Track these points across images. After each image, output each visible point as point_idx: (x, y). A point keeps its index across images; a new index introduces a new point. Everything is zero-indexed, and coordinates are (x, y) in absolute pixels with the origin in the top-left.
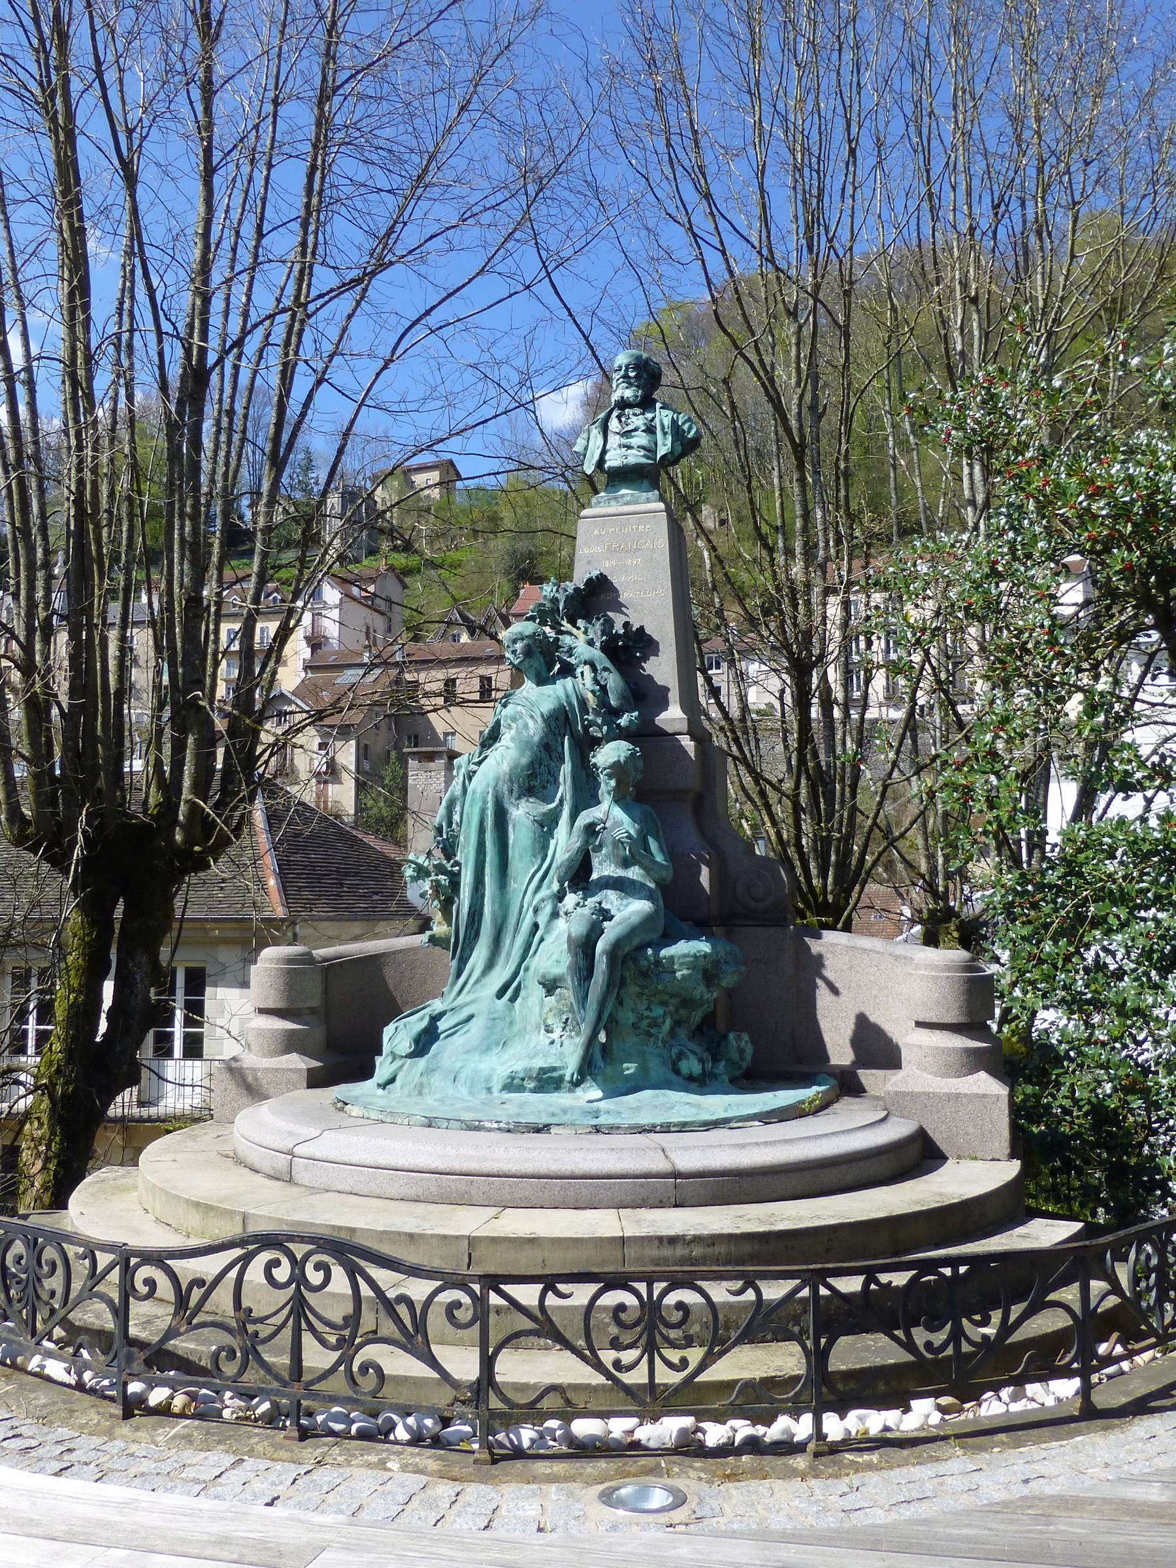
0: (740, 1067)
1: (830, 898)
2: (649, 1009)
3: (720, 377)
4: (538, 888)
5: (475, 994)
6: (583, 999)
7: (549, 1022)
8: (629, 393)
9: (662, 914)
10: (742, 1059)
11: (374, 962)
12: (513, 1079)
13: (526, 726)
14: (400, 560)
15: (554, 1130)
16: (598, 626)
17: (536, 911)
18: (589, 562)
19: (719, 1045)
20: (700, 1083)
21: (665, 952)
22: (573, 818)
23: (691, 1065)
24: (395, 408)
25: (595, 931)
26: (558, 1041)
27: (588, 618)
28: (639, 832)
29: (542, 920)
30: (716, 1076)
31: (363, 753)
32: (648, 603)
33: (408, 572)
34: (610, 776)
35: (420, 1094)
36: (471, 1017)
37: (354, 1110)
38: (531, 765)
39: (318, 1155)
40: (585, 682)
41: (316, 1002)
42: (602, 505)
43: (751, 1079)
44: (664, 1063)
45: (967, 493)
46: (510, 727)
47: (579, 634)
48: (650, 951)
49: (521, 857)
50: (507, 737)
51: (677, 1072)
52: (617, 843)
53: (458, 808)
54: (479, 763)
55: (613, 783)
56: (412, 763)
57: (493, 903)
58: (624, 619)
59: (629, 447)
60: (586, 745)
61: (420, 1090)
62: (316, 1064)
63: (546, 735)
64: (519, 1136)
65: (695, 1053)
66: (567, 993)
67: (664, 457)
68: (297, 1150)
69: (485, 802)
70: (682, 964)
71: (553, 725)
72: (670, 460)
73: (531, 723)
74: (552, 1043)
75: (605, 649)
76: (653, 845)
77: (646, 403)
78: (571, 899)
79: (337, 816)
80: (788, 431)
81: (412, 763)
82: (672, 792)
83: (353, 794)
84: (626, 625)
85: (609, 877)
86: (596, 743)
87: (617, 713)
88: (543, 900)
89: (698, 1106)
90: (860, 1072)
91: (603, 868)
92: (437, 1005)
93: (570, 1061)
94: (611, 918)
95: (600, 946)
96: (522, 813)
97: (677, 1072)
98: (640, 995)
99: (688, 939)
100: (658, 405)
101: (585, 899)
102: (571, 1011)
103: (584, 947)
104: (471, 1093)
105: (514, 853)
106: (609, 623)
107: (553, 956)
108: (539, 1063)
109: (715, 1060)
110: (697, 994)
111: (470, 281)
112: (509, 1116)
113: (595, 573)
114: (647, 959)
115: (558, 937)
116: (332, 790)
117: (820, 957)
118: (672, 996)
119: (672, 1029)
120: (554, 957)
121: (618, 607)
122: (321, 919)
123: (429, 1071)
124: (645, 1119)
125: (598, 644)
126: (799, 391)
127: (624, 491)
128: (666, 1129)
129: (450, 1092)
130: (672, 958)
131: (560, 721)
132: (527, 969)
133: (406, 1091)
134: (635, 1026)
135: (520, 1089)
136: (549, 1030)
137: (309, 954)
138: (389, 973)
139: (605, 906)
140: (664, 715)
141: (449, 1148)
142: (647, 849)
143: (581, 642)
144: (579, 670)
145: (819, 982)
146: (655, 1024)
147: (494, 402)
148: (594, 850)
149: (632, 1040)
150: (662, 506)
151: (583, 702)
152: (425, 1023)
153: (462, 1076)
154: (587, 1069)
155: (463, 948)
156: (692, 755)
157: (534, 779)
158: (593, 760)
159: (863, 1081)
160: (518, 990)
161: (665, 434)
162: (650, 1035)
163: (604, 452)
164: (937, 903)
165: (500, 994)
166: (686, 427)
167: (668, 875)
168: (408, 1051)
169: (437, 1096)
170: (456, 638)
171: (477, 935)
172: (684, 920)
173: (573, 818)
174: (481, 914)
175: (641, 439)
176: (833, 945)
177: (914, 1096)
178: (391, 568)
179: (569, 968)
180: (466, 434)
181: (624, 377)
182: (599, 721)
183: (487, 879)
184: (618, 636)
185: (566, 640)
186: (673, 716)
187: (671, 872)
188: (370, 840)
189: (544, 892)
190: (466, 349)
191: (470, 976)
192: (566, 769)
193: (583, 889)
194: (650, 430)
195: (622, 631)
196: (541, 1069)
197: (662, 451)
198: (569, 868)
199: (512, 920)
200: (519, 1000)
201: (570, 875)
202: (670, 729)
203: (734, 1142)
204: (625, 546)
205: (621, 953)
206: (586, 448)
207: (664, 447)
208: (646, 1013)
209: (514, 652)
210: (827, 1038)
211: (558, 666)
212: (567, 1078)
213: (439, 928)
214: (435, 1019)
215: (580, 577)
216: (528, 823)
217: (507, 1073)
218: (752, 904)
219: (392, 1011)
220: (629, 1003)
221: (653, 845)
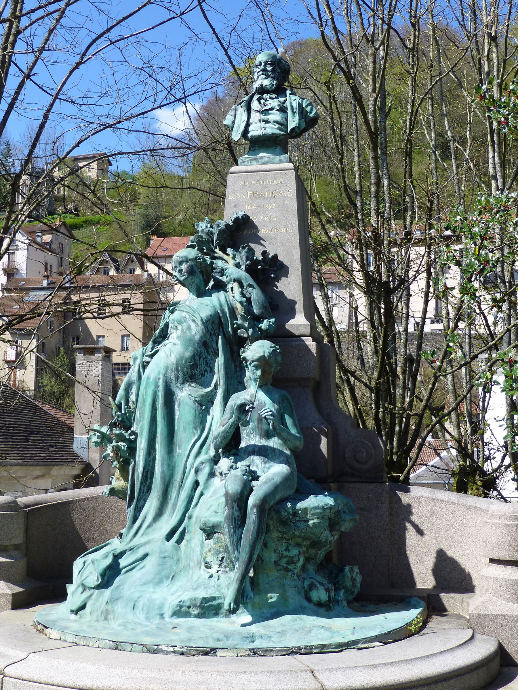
0: (353, 593)
1: (395, 458)
2: (287, 550)
3: (323, 80)
4: (199, 453)
5: (151, 536)
6: (237, 543)
7: (208, 560)
8: (267, 83)
9: (295, 474)
10: (354, 586)
11: (64, 507)
12: (181, 607)
13: (189, 328)
14: (70, 220)
15: (219, 653)
16: (244, 253)
17: (197, 471)
18: (236, 206)
19: (337, 576)
20: (326, 609)
21: (301, 505)
22: (226, 399)
23: (320, 594)
24: (79, 101)
25: (246, 490)
26: (215, 576)
27: (236, 249)
28: (279, 411)
29: (202, 478)
30: (338, 602)
31: (41, 348)
32: (280, 236)
33: (75, 227)
34: (257, 367)
35: (106, 619)
36: (146, 556)
37: (54, 634)
38: (193, 357)
39: (25, 676)
40: (234, 295)
41: (19, 540)
42: (246, 163)
43: (365, 602)
44: (299, 593)
45: (491, 171)
46: (176, 328)
47: (229, 259)
48: (289, 505)
49: (185, 429)
50: (174, 336)
51: (309, 599)
52: (260, 419)
53: (134, 390)
54: (152, 356)
55: (259, 373)
56: (79, 356)
57: (162, 464)
58: (262, 249)
59: (267, 122)
60: (235, 344)
61: (106, 616)
62: (19, 589)
63: (205, 335)
64: (191, 658)
65: (322, 584)
66: (225, 538)
67: (293, 130)
68: (7, 671)
69: (157, 386)
70: (313, 515)
71: (210, 327)
72: (297, 133)
73: (193, 325)
74: (211, 577)
75: (247, 270)
76: (289, 421)
77: (279, 91)
78: (225, 463)
79: (24, 391)
80: (367, 122)
81: (79, 356)
82: (301, 379)
83: (33, 376)
84: (264, 253)
85: (255, 446)
86: (242, 342)
87: (259, 319)
88: (202, 463)
89: (329, 629)
90: (442, 595)
91: (250, 438)
92: (116, 545)
93: (228, 596)
94: (257, 478)
95: (252, 501)
96: (186, 395)
97: (309, 599)
98: (280, 539)
99: (316, 494)
100: (288, 92)
101: (236, 462)
102: (227, 550)
103: (239, 502)
104: (147, 618)
105: (179, 426)
106: (251, 251)
107: (212, 506)
108: (202, 594)
109: (337, 590)
110: (323, 537)
111: (140, 9)
112: (182, 641)
113: (240, 214)
114: (287, 511)
115: (215, 492)
116: (19, 373)
117: (409, 506)
118: (304, 539)
119: (304, 566)
120: (213, 509)
121: (258, 240)
122: (12, 465)
123: (112, 600)
124: (292, 643)
125: (243, 267)
126: (375, 95)
127: (262, 154)
128: (309, 651)
129: (131, 617)
130: (306, 509)
131: (215, 324)
132: (190, 517)
133: (94, 617)
134: (276, 563)
135: (188, 615)
136: (208, 566)
137: (15, 502)
138: (76, 516)
139: (253, 468)
140: (292, 322)
141: (135, 671)
142: (284, 423)
143: (230, 265)
144: (229, 286)
145: (408, 525)
146: (292, 561)
147: (152, 99)
148: (243, 425)
149: (274, 574)
150: (291, 165)
151: (233, 311)
152: (109, 560)
153: (140, 605)
154: (241, 599)
155: (136, 498)
156: (314, 352)
157: (195, 369)
158: (243, 355)
159: (445, 602)
160: (183, 534)
161: (294, 113)
162: (288, 570)
163: (248, 125)
164: (465, 461)
165: (169, 537)
166: (308, 109)
167: (300, 444)
168: (96, 583)
169: (120, 621)
170: (106, 272)
171: (149, 489)
172: (308, 478)
173: (226, 399)
174: (153, 473)
176: (419, 497)
177: (493, 618)
178: (64, 224)
179: (226, 518)
180: (133, 120)
182: (246, 325)
183: (158, 446)
184: (257, 262)
185: (219, 263)
186: (298, 323)
187: (302, 442)
188: (46, 408)
189: (203, 457)
190: (135, 56)
191: (143, 521)
192: (220, 361)
193: (234, 455)
194: (283, 110)
195: (261, 258)
196: (204, 599)
197: (292, 125)
198: (224, 438)
199: (178, 478)
200: (184, 542)
201: (223, 445)
202: (297, 332)
203: (366, 663)
204: (265, 195)
205: (267, 507)
206: (233, 123)
208: (285, 553)
209: (180, 271)
210: (415, 568)
211: (212, 283)
212: (226, 607)
213: (118, 483)
214: (117, 557)
215: (229, 215)
216: (191, 402)
217: (176, 602)
218: (358, 466)
219: (81, 549)
220: (272, 545)
221: (289, 421)
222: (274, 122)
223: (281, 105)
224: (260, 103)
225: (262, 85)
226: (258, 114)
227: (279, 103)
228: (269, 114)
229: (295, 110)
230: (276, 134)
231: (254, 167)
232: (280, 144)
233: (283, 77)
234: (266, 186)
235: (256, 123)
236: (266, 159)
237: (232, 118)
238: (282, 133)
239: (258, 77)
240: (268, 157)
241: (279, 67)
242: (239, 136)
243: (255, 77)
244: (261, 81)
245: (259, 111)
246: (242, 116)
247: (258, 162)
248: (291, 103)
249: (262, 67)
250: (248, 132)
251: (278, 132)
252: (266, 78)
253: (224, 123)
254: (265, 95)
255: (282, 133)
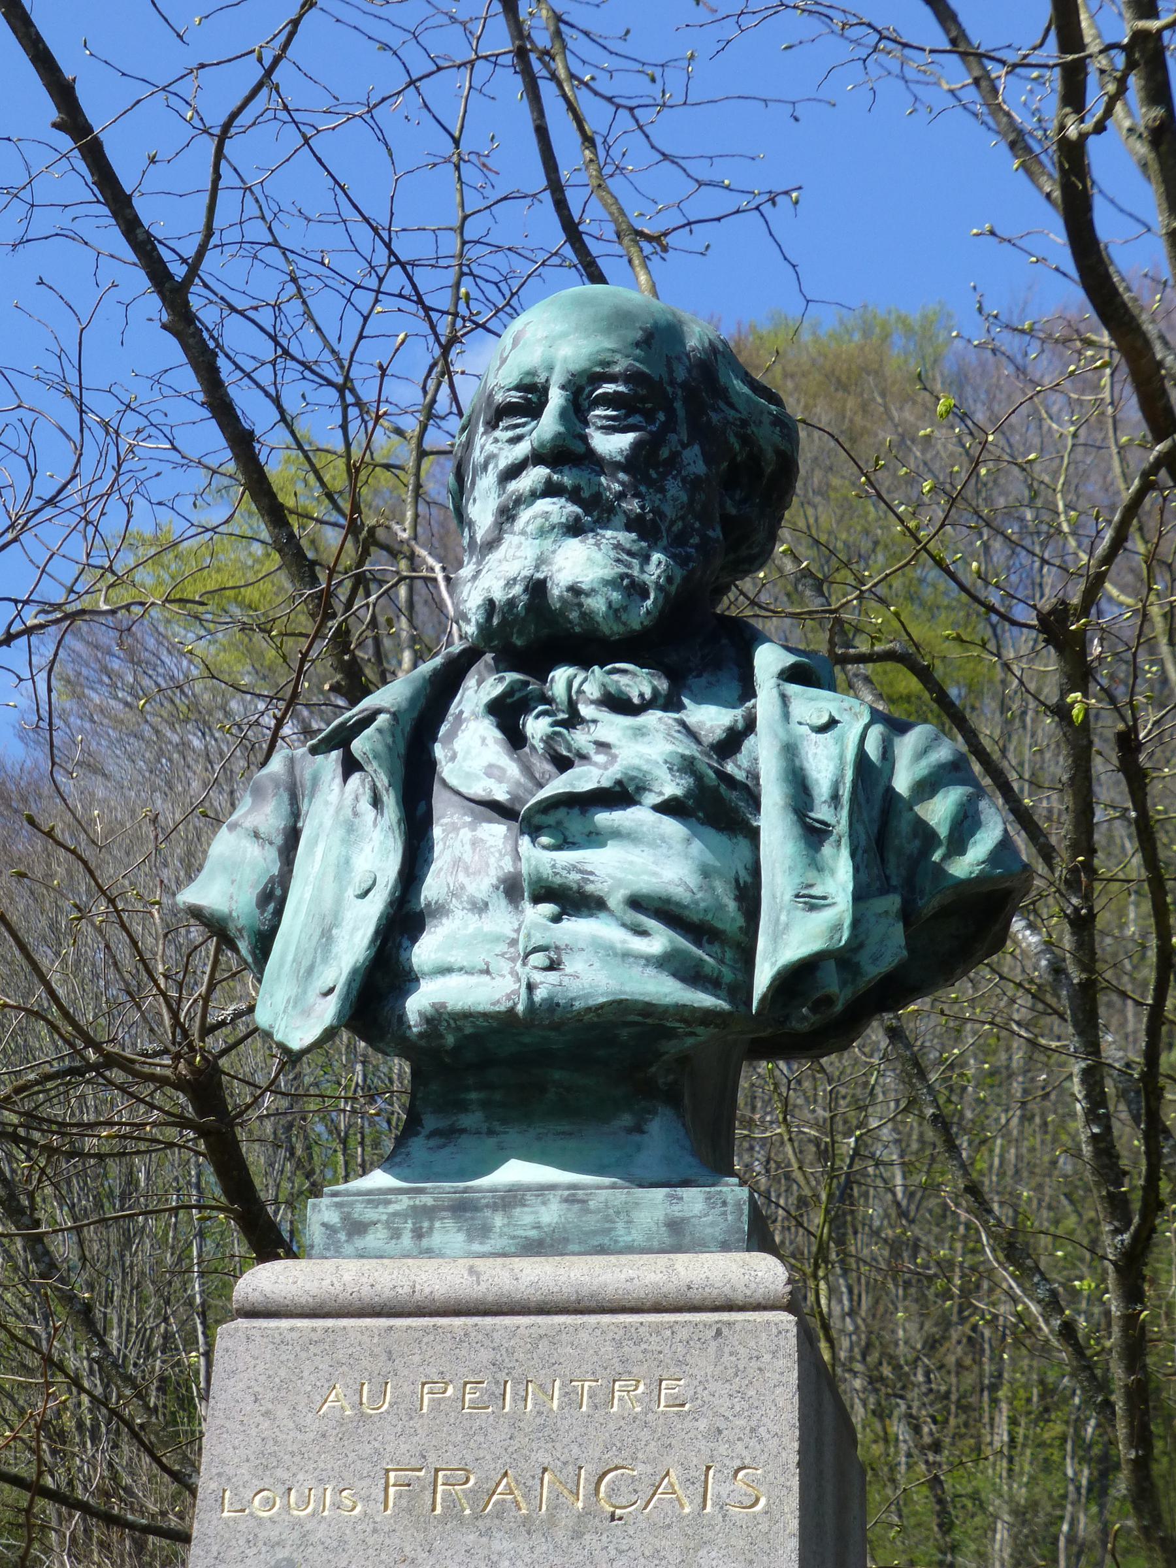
8: (582, 565)
42: (374, 1242)
59: (572, 900)
67: (797, 978)
72: (819, 1010)
77: (691, 644)
100: (768, 660)
127: (516, 1172)
150: (767, 1272)
161: (814, 835)
163: (404, 920)
166: (939, 811)
175: (651, 855)
181: (554, 455)
194: (716, 804)
197: (788, 938)
206: (274, 897)
207: (805, 914)
222: (636, 903)
223: (707, 764)
224: (515, 739)
225: (537, 588)
226: (497, 832)
227: (687, 748)
228: (595, 838)
229: (822, 812)
230: (648, 1010)
231: (449, 1267)
232: (673, 1098)
233: (727, 522)
234: (547, 1430)
235: (480, 907)
236: (550, 1214)
237: (260, 861)
238: (704, 1000)
239: (507, 515)
240: (573, 1197)
241: (701, 432)
242: (327, 1011)
243: (482, 511)
244: (535, 550)
245: (501, 811)
246: (349, 849)
247: (484, 1231)
248: (790, 751)
249: (548, 425)
250: (407, 980)
251: (666, 990)
252: (574, 529)
253: (189, 896)
254: (560, 676)
255: (704, 1000)
